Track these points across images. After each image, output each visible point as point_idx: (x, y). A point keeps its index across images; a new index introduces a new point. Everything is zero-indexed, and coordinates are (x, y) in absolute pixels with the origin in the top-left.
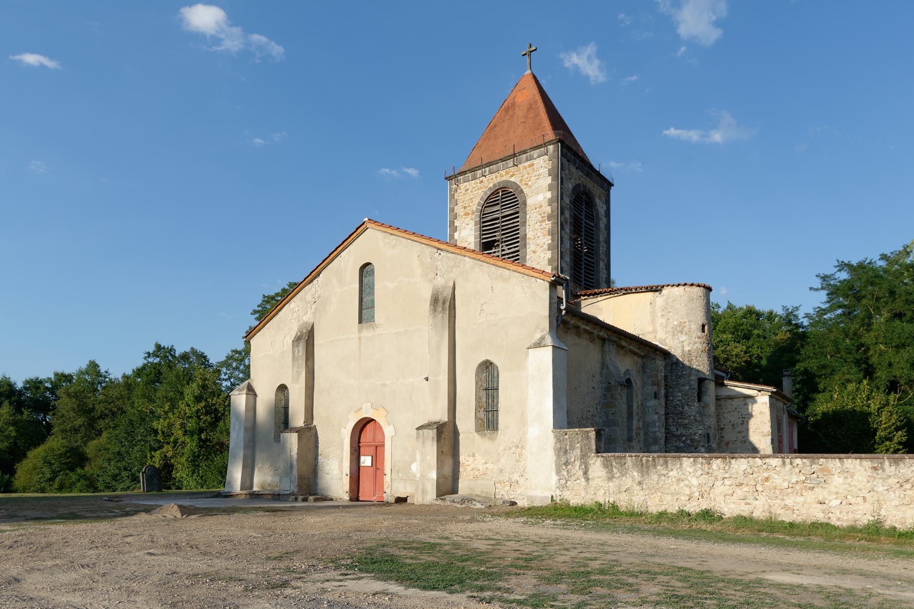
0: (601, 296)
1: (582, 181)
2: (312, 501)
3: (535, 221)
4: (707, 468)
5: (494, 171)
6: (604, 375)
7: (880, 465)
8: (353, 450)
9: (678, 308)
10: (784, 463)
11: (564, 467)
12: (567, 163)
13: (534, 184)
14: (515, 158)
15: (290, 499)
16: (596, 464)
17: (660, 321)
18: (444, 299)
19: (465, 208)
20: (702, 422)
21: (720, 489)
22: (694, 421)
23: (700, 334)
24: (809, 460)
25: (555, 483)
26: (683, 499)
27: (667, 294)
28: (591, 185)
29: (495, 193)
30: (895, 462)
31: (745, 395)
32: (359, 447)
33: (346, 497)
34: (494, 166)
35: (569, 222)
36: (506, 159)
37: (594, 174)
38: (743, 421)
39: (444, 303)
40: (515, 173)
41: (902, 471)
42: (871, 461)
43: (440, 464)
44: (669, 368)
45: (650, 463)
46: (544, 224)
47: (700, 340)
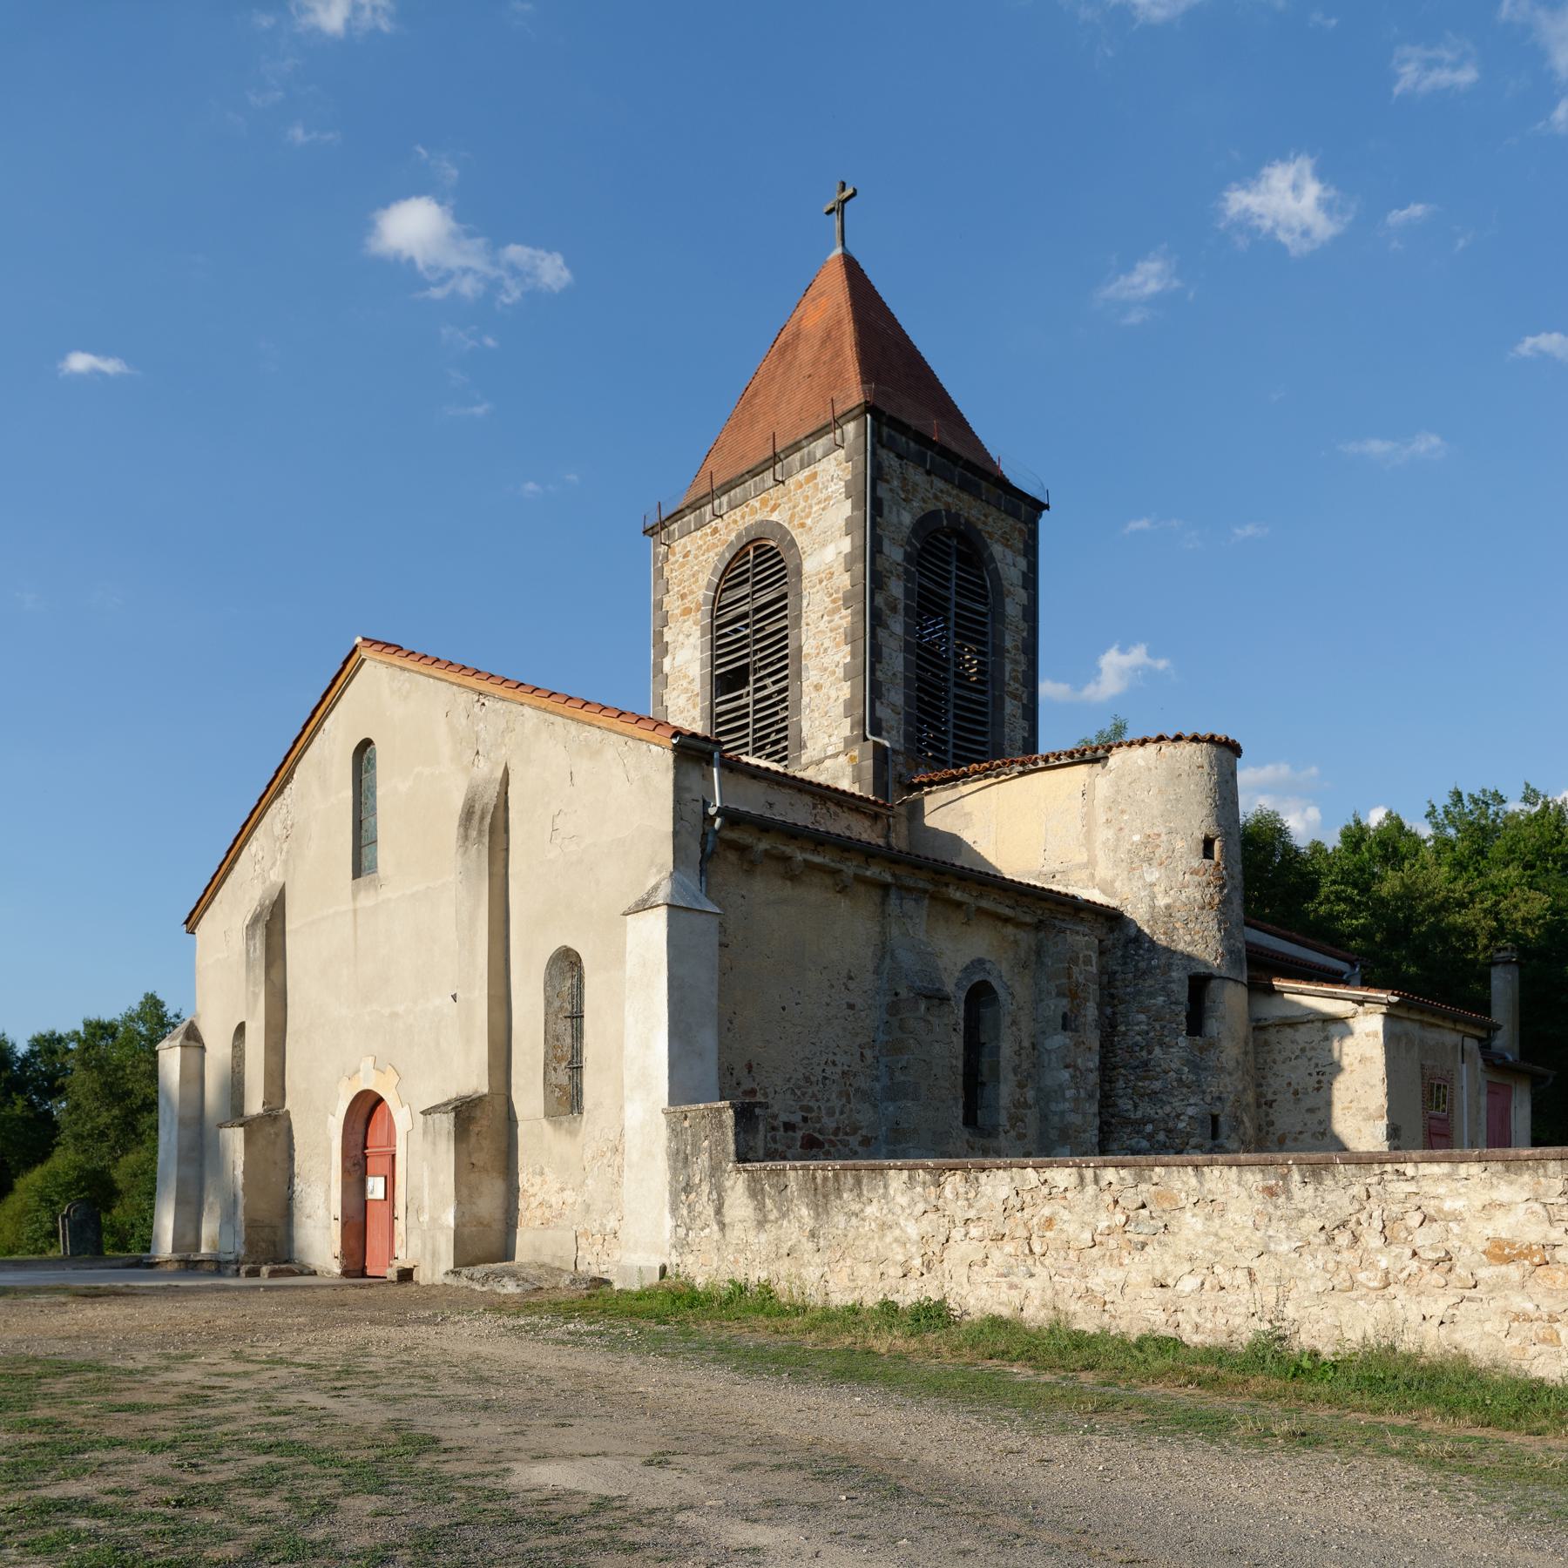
0: (964, 783)
1: (947, 504)
2: (266, 1276)
3: (819, 611)
4: (933, 1196)
5: (738, 503)
6: (885, 975)
7: (1281, 1183)
8: (348, 1165)
9: (1143, 801)
10: (1082, 1178)
11: (683, 1197)
12: (895, 462)
13: (818, 522)
14: (778, 467)
15: (229, 1272)
16: (736, 1188)
17: (1104, 834)
18: (483, 809)
19: (683, 597)
20: (1197, 1087)
21: (961, 1249)
22: (1175, 1084)
23: (1196, 862)
24: (1133, 1171)
25: (668, 1236)
26: (893, 1274)
27: (1118, 767)
28: (970, 509)
29: (741, 554)
30: (1314, 1174)
31: (1324, 1014)
32: (365, 1157)
33: (336, 1268)
34: (737, 490)
35: (901, 606)
36: (759, 469)
37: (984, 484)
38: (1319, 1082)
39: (482, 818)
40: (779, 501)
41: (1329, 1198)
42: (1262, 1171)
43: (465, 1192)
44: (1120, 953)
45: (830, 1184)
46: (836, 617)
47: (1197, 878)
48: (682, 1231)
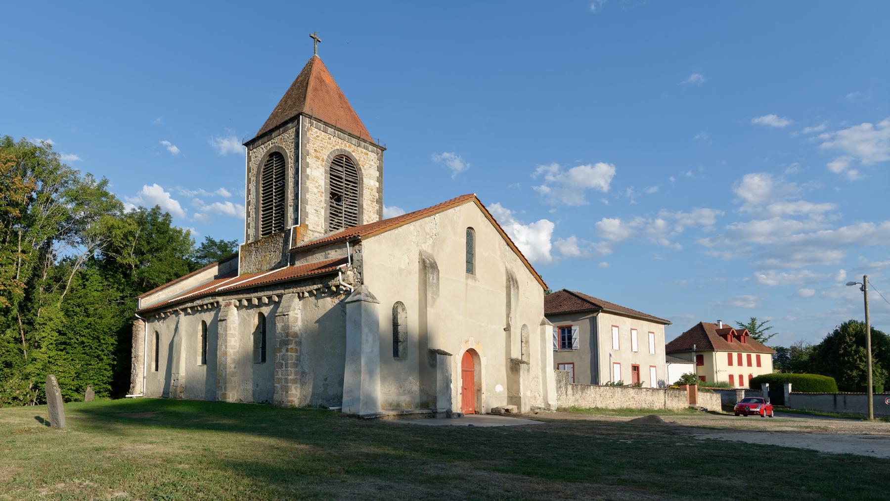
48: (559, 397)
